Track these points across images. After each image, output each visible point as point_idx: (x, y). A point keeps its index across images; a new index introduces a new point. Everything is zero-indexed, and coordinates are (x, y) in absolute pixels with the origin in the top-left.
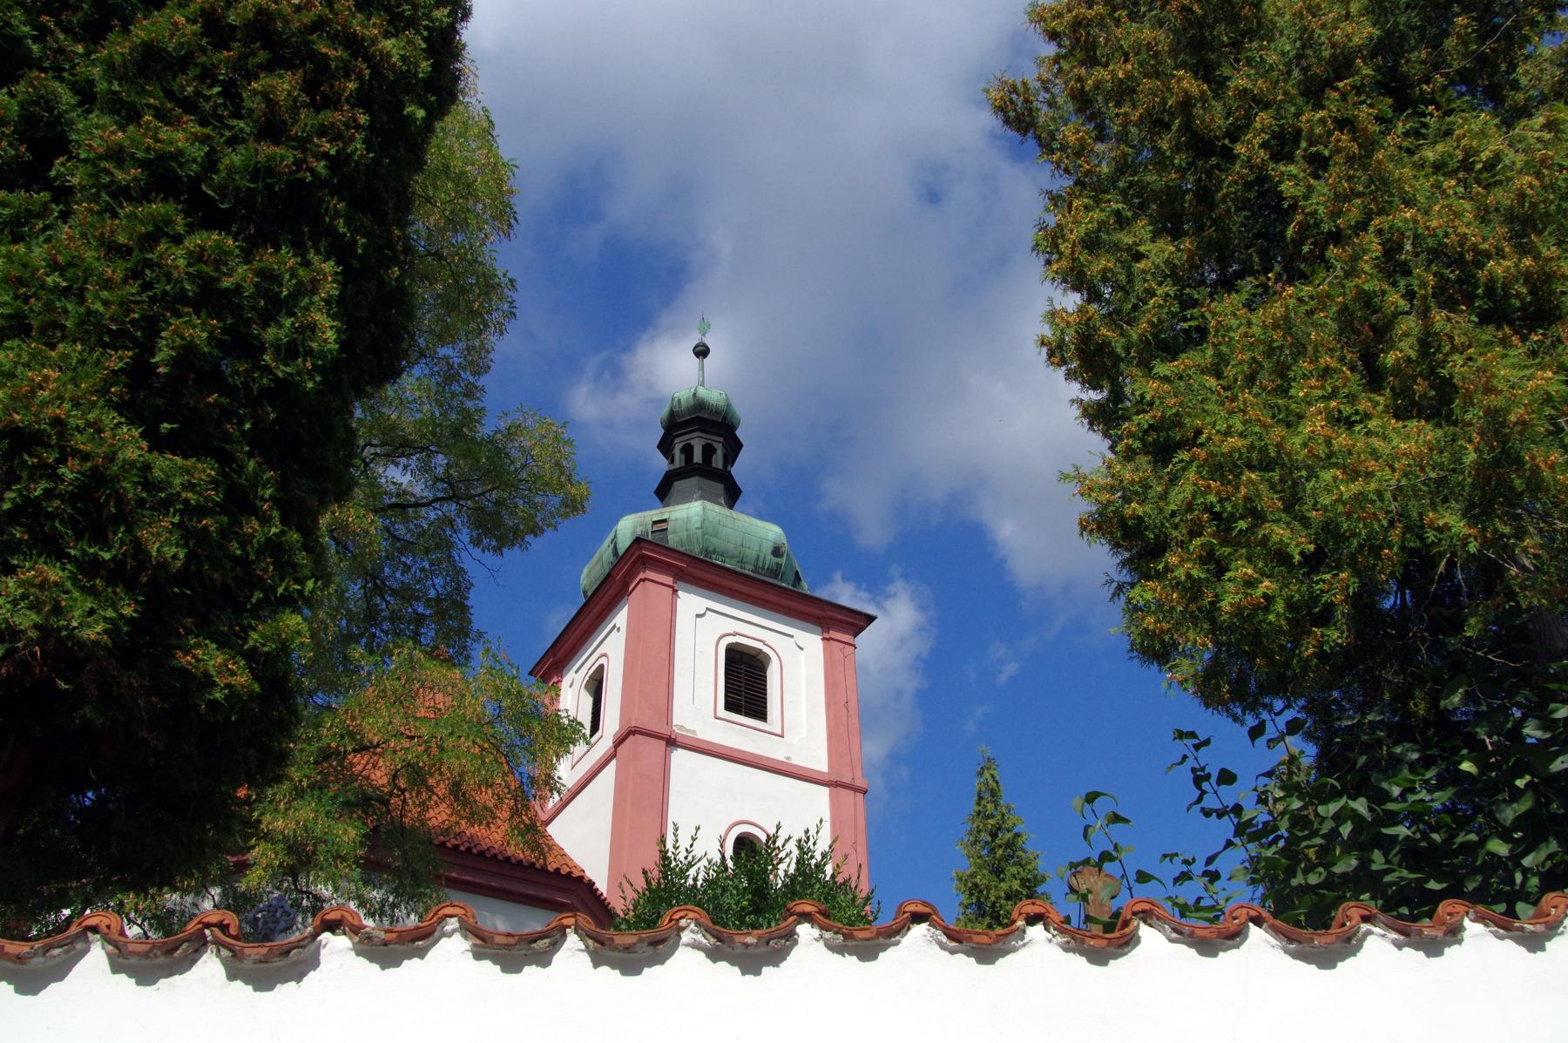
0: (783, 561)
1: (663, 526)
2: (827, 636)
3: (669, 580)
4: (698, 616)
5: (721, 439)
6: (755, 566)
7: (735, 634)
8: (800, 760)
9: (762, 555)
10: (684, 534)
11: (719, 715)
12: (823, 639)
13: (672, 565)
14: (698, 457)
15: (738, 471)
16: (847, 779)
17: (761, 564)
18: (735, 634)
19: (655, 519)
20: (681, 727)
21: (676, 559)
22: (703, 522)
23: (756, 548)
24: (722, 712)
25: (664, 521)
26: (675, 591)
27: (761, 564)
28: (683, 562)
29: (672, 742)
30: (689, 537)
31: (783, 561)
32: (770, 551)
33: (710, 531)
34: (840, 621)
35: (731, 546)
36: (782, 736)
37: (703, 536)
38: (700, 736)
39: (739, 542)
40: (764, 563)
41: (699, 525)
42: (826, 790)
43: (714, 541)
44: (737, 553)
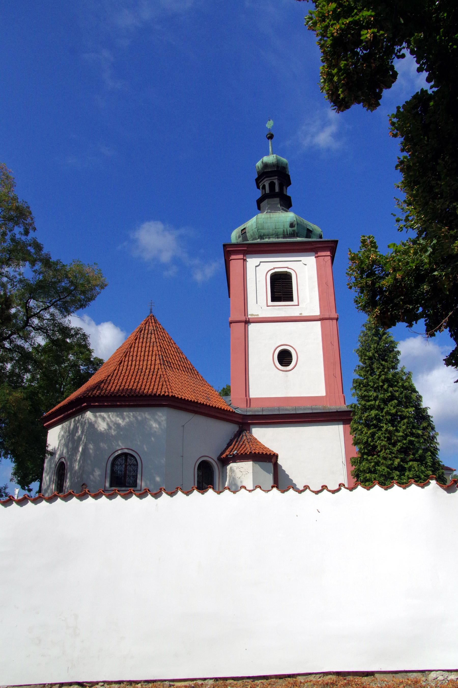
0: (295, 228)
1: (244, 231)
2: (317, 255)
3: (241, 256)
4: (256, 266)
5: (276, 177)
6: (284, 235)
7: (274, 269)
8: (306, 313)
9: (285, 230)
10: (251, 232)
11: (269, 305)
12: (316, 257)
13: (240, 250)
14: (277, 190)
15: (290, 191)
16: (327, 316)
17: (286, 233)
18: (274, 269)
19: (242, 229)
20: (252, 315)
21: (236, 248)
22: (257, 225)
23: (282, 227)
24: (270, 303)
25: (245, 229)
26: (245, 260)
27: (286, 233)
28: (244, 247)
29: (247, 322)
30: (253, 233)
31: (295, 228)
32: (289, 226)
33: (260, 228)
34: (322, 247)
35: (271, 231)
36: (298, 305)
37: (258, 230)
38: (261, 316)
39: (274, 228)
40: (287, 232)
41: (255, 227)
42: (319, 323)
43: (263, 231)
44: (274, 232)
